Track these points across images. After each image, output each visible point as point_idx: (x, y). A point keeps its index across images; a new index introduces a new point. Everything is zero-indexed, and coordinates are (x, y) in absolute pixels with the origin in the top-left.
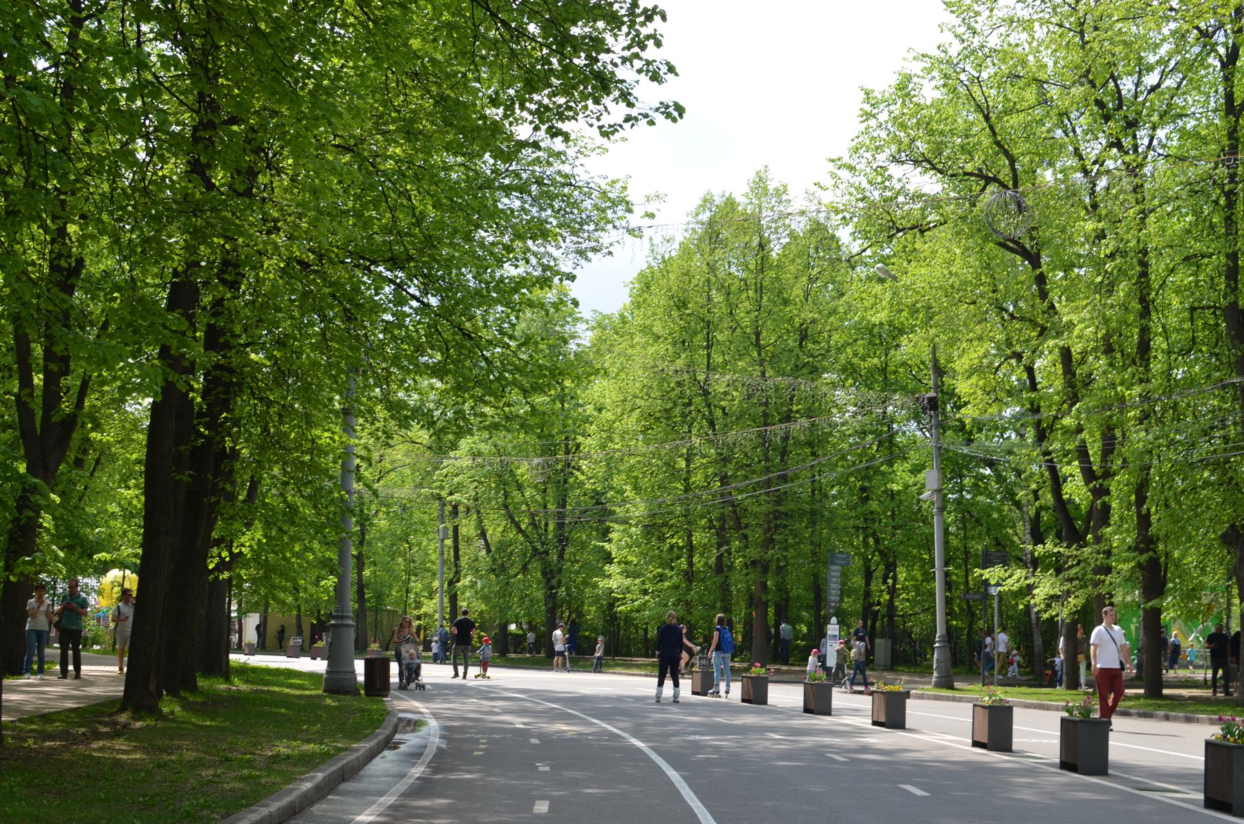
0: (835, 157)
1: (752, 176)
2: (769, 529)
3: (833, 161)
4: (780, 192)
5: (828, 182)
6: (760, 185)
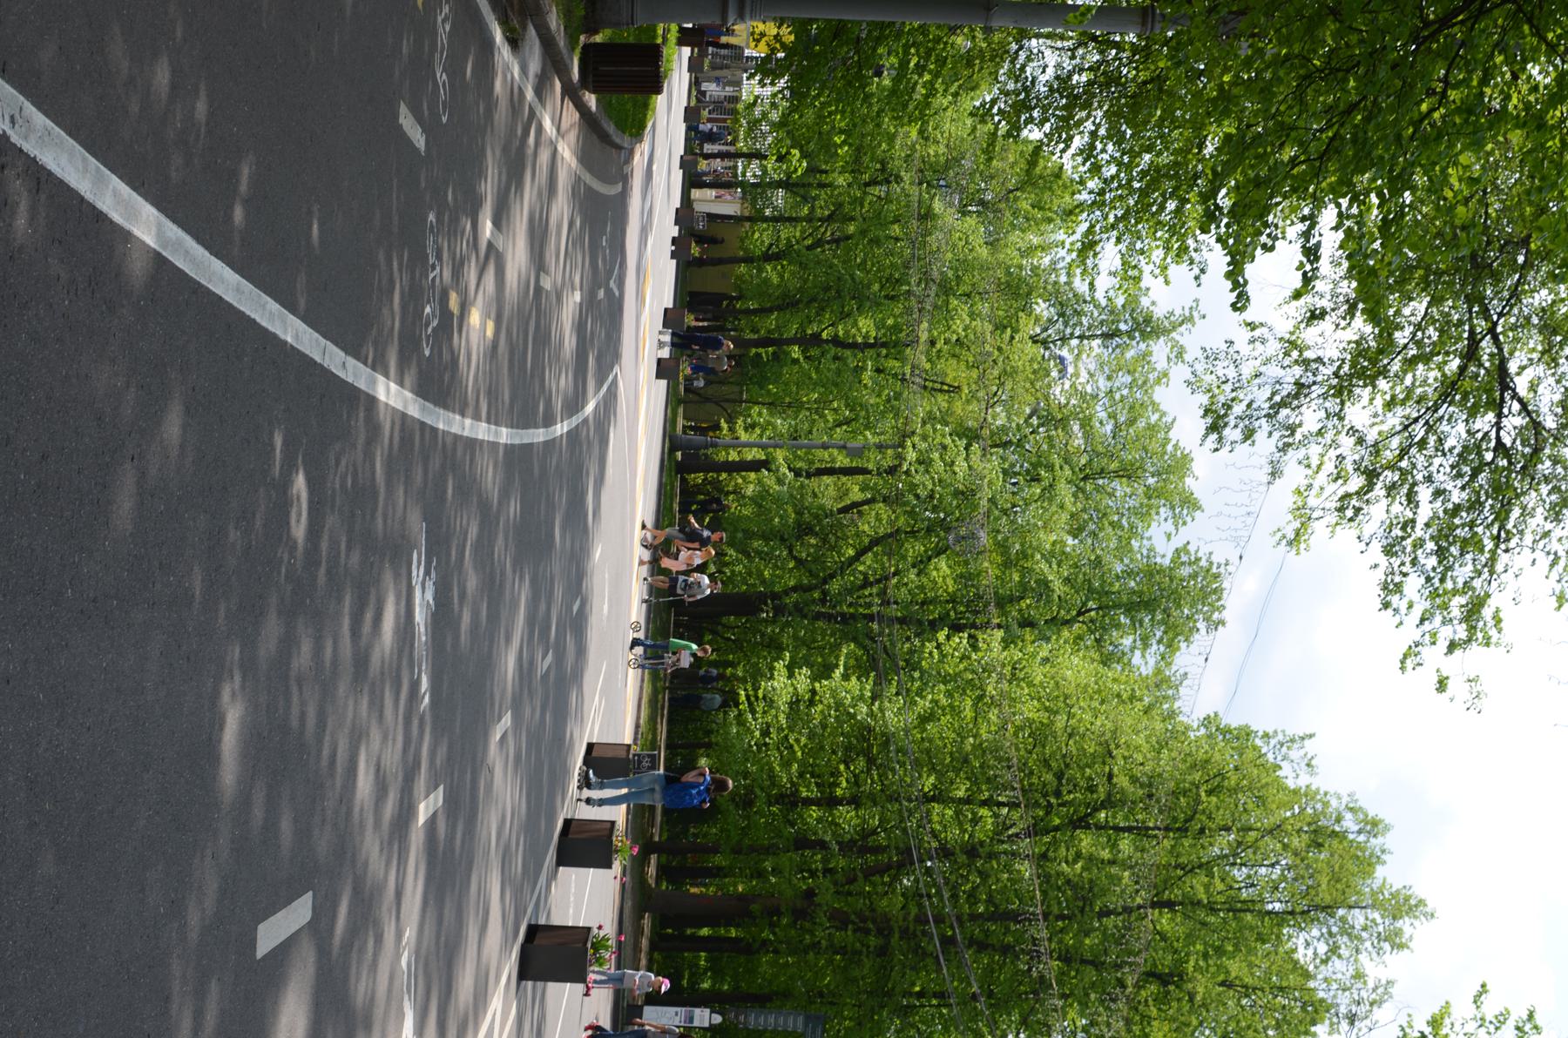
0: (1539, 1019)
1: (1419, 891)
2: (864, 920)
3: (1531, 1016)
4: (1395, 941)
5: (1490, 1008)
6: (1402, 906)
